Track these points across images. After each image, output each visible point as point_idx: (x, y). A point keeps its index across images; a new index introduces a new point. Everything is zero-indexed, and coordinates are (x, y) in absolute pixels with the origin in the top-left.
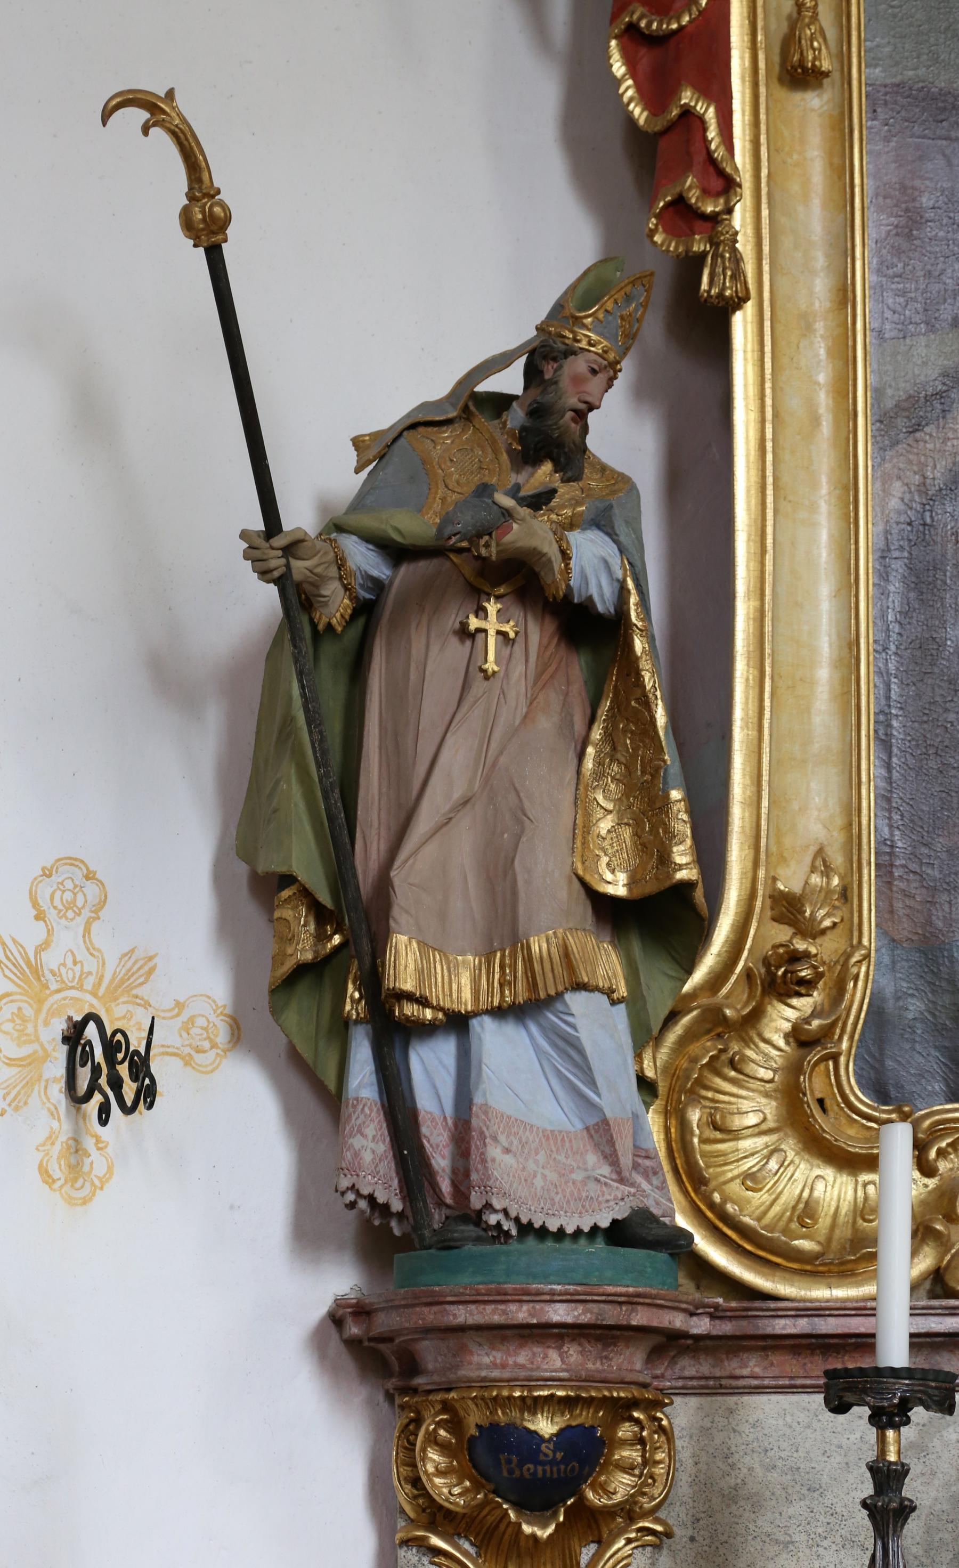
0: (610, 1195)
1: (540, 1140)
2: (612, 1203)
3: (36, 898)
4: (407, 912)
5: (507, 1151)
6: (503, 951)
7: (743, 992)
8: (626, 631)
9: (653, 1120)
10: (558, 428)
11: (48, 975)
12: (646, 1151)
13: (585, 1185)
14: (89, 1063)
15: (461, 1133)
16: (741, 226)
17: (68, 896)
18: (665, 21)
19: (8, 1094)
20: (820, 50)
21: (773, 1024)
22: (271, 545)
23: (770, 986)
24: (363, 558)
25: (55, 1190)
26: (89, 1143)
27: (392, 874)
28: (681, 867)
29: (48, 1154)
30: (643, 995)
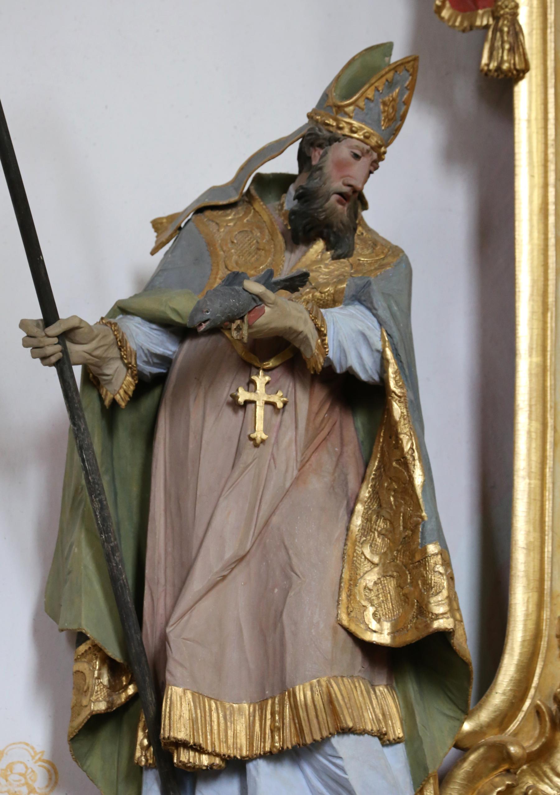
4: (182, 665)
6: (273, 698)
7: (534, 728)
10: (324, 211)
22: (52, 334)
24: (145, 339)
27: (168, 630)
28: (437, 617)
30: (419, 736)
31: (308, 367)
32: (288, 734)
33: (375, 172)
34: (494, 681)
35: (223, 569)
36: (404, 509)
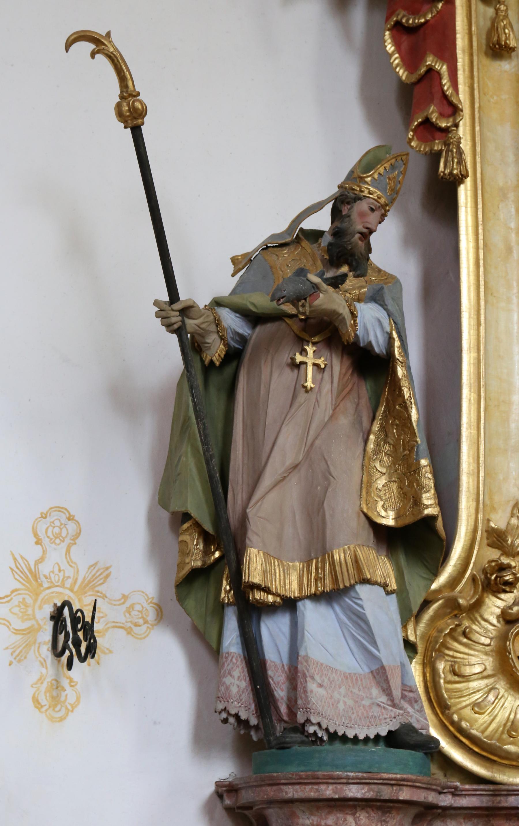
0: (387, 715)
1: (342, 679)
2: (388, 720)
3: (37, 531)
4: (257, 534)
5: (321, 686)
6: (317, 559)
7: (471, 590)
8: (393, 363)
9: (415, 670)
10: (350, 244)
11: (43, 579)
12: (410, 687)
13: (371, 708)
14: (64, 633)
15: (293, 674)
16: (463, 135)
17: (57, 530)
18: (417, 17)
19: (14, 652)
20: (509, 35)
21: (490, 610)
22: (176, 313)
23: (487, 586)
24: (231, 321)
25: (42, 712)
26: (65, 683)
27: (248, 511)
28: (427, 507)
29: (38, 689)
31: (343, 340)
32: (328, 582)
33: (382, 223)
34: (448, 558)
35: (284, 473)
36: (404, 437)
